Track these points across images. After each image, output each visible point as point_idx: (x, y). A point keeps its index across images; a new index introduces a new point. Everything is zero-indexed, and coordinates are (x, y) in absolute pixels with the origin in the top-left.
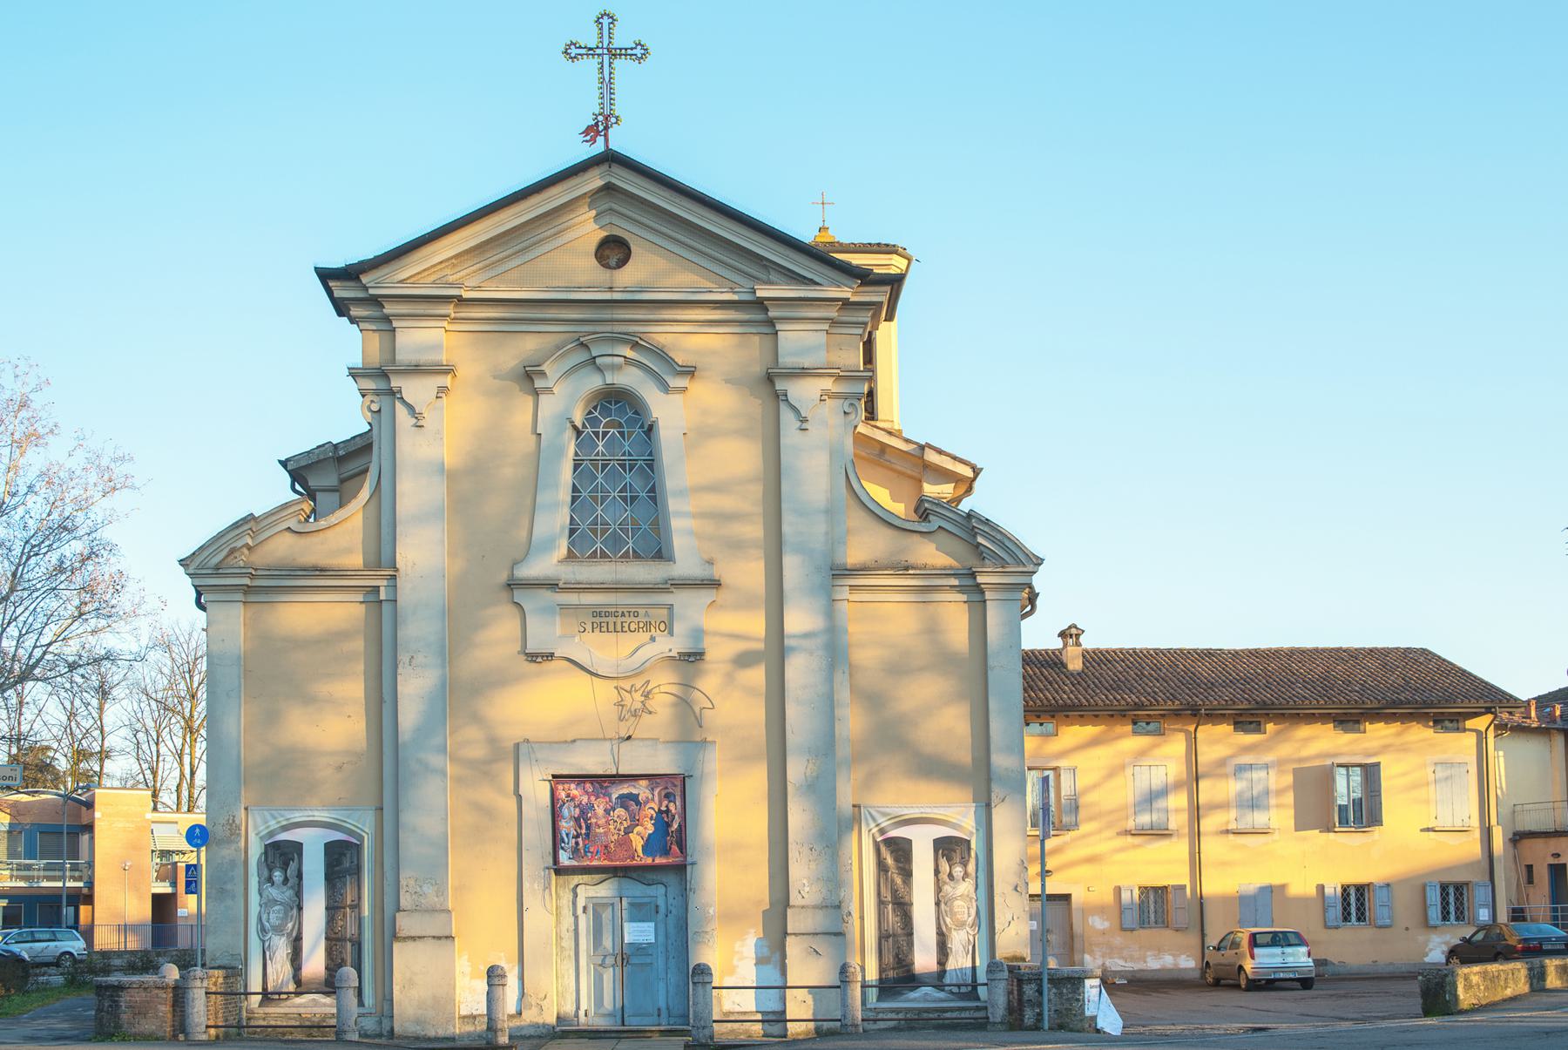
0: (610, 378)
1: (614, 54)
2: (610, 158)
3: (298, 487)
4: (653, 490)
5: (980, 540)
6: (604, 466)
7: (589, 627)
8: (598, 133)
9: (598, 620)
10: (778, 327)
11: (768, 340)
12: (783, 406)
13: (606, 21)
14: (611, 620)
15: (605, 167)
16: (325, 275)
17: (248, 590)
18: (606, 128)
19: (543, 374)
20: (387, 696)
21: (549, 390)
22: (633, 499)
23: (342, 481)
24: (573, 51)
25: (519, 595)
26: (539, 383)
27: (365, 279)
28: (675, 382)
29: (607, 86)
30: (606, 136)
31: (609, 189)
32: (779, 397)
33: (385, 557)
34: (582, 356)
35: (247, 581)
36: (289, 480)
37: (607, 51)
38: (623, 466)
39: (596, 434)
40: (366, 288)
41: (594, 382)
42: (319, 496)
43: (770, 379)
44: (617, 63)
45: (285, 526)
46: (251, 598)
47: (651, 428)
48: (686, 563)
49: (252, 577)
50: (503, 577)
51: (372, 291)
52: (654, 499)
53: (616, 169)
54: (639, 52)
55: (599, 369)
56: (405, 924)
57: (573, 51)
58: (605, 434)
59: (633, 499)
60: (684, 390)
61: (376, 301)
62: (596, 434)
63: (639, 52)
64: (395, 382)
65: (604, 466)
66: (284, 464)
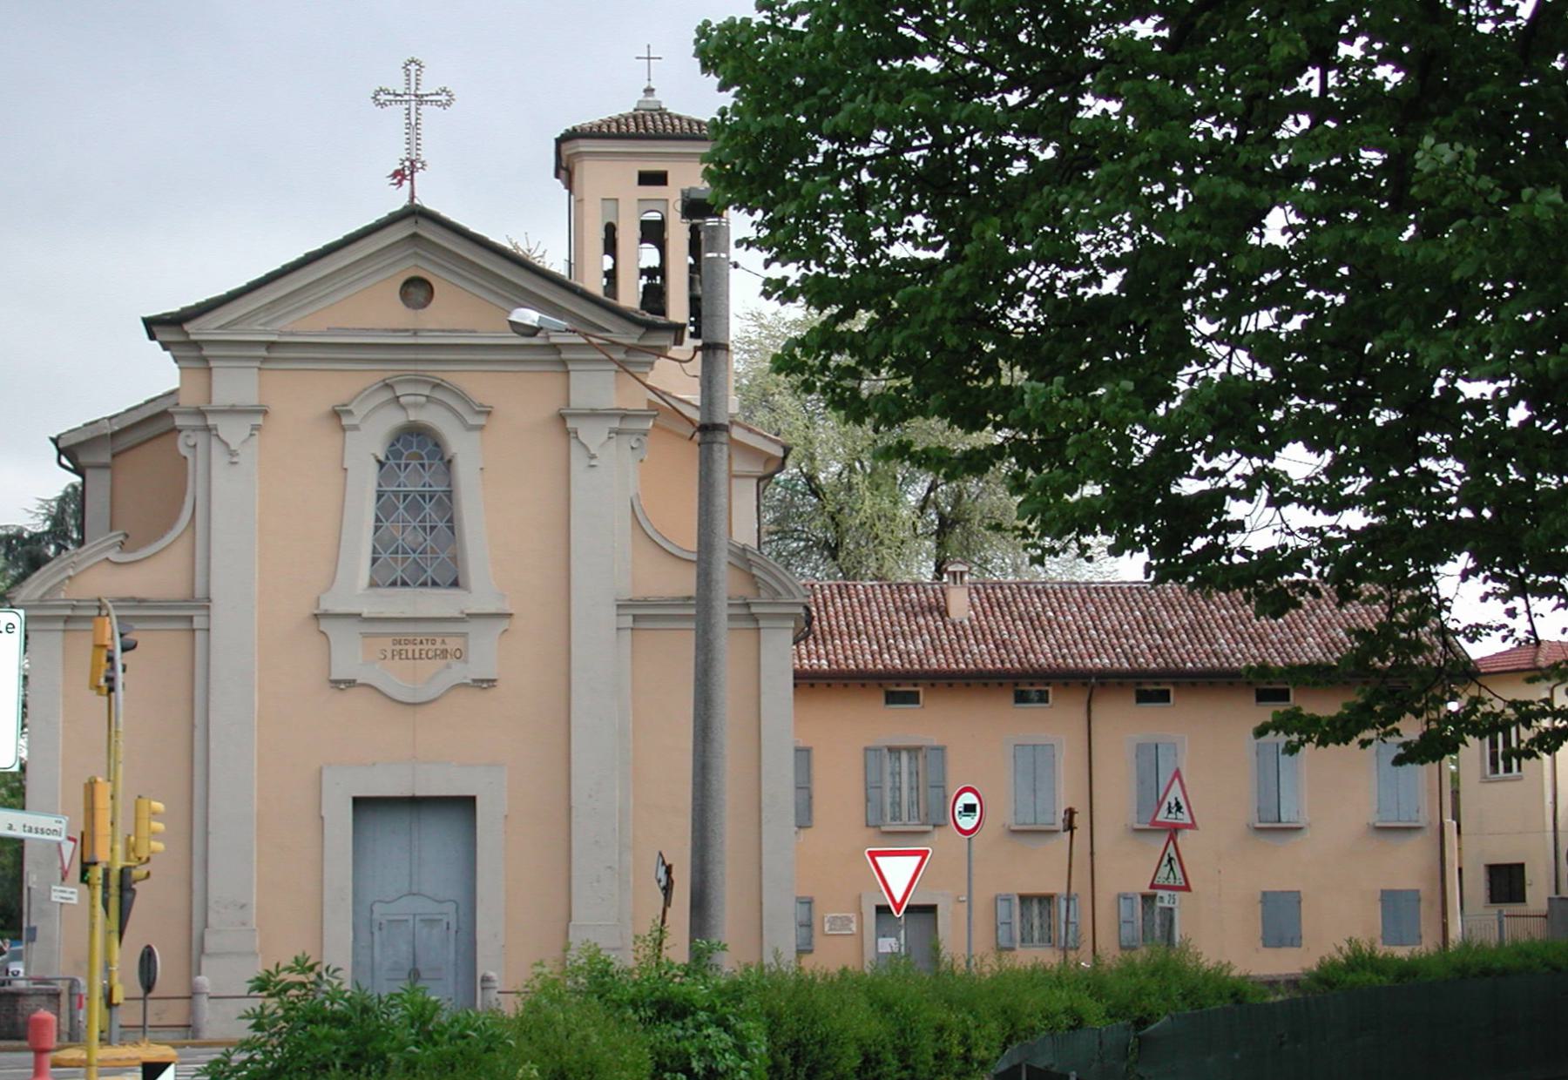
0: (413, 416)
1: (420, 99)
2: (413, 212)
3: (64, 461)
4: (451, 520)
5: (755, 571)
6: (406, 497)
7: (389, 655)
8: (404, 177)
9: (398, 647)
10: (570, 367)
11: (561, 378)
12: (573, 442)
13: (413, 67)
14: (410, 647)
15: (412, 220)
16: (153, 325)
17: (68, 619)
18: (412, 173)
19: (350, 412)
20: (198, 720)
21: (355, 428)
22: (433, 528)
23: (114, 456)
24: (382, 98)
25: (325, 625)
26: (346, 421)
27: (187, 327)
28: (473, 420)
29: (413, 127)
30: (412, 181)
31: (414, 236)
32: (569, 434)
33: (199, 593)
34: (386, 395)
35: (68, 612)
36: (55, 452)
37: (412, 98)
38: (423, 497)
39: (399, 466)
40: (187, 334)
41: (396, 419)
42: (89, 473)
43: (562, 417)
44: (423, 108)
45: (103, 556)
46: (71, 626)
47: (450, 461)
48: (481, 594)
49: (74, 607)
50: (310, 610)
51: (193, 337)
52: (452, 529)
53: (421, 221)
54: (445, 99)
55: (403, 407)
56: (211, 942)
57: (382, 98)
58: (407, 466)
59: (433, 528)
60: (481, 428)
61: (197, 345)
62: (399, 466)
63: (445, 99)
64: (211, 421)
65: (406, 497)
66: (55, 441)
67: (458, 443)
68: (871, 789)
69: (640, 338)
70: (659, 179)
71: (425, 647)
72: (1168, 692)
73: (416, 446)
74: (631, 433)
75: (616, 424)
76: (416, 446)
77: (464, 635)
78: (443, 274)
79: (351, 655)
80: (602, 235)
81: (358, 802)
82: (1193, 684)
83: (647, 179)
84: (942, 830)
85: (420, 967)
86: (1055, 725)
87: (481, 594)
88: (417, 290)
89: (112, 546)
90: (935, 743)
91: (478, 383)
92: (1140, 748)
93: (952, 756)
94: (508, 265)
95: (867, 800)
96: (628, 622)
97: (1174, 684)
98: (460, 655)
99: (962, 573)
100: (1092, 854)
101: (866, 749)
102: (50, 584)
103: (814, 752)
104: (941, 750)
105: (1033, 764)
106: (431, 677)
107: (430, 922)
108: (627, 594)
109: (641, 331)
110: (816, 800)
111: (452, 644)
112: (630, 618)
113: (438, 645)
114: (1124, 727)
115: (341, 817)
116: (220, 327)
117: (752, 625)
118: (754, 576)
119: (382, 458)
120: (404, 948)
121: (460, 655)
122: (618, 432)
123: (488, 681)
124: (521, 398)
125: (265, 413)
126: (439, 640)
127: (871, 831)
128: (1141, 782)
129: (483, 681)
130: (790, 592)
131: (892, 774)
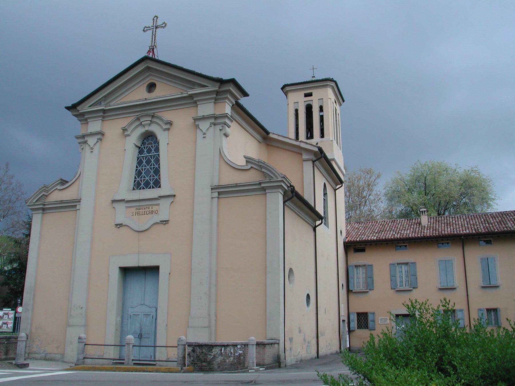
0: (147, 128)
7: (134, 214)
9: (137, 211)
14: (141, 211)
21: (129, 135)
27: (78, 108)
32: (197, 127)
41: (141, 130)
55: (144, 126)
60: (168, 129)
61: (83, 114)
63: (164, 25)
67: (162, 136)
68: (393, 277)
69: (219, 88)
70: (310, 95)
71: (146, 210)
72: (491, 241)
73: (149, 138)
74: (219, 124)
75: (213, 121)
76: (149, 138)
77: (158, 205)
78: (159, 80)
79: (122, 214)
80: (295, 112)
81: (125, 271)
82: (498, 236)
83: (306, 95)
84: (416, 290)
85: (143, 333)
86: (452, 255)
87: (165, 189)
88: (151, 87)
89: (58, 184)
90: (413, 261)
91: (167, 115)
92: (482, 259)
93: (418, 265)
94: (175, 70)
95: (391, 280)
96: (216, 195)
97: (492, 237)
98: (157, 212)
99: (424, 211)
100: (467, 295)
101: (390, 264)
102: (38, 198)
103: (374, 266)
104: (414, 263)
105: (446, 267)
106: (147, 221)
107: (147, 315)
108: (216, 183)
109: (218, 84)
110: (374, 280)
111: (155, 208)
112: (217, 193)
113: (151, 209)
114: (476, 255)
115: (116, 274)
116: (90, 106)
117: (263, 192)
118: (263, 172)
119: (139, 145)
120: (138, 325)
121: (157, 212)
122: (215, 124)
123: (165, 221)
124: (181, 118)
125: (103, 135)
126: (151, 207)
127: (393, 290)
128: (483, 270)
129: (164, 221)
130: (276, 177)
131: (399, 272)
